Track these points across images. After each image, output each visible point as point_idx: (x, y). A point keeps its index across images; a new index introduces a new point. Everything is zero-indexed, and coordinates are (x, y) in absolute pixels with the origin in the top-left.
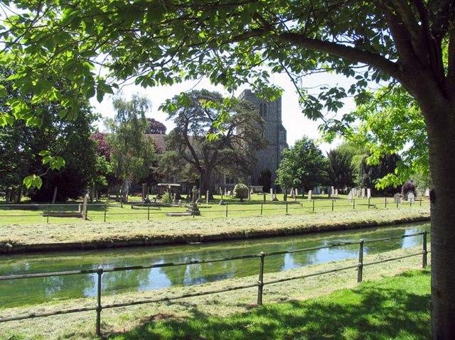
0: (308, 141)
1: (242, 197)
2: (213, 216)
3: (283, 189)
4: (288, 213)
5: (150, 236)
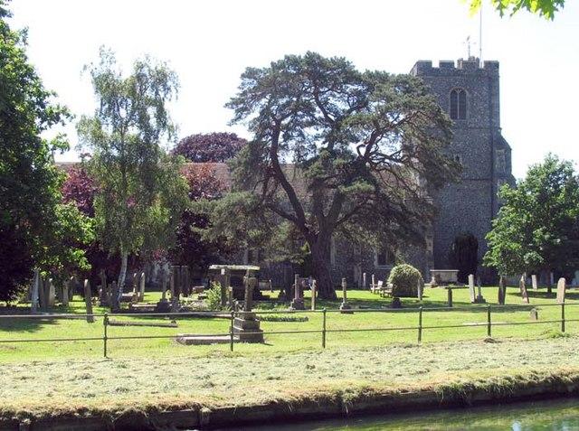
0: (557, 166)
1: (403, 297)
2: (295, 342)
3: (502, 275)
4: (494, 335)
5: (38, 414)
